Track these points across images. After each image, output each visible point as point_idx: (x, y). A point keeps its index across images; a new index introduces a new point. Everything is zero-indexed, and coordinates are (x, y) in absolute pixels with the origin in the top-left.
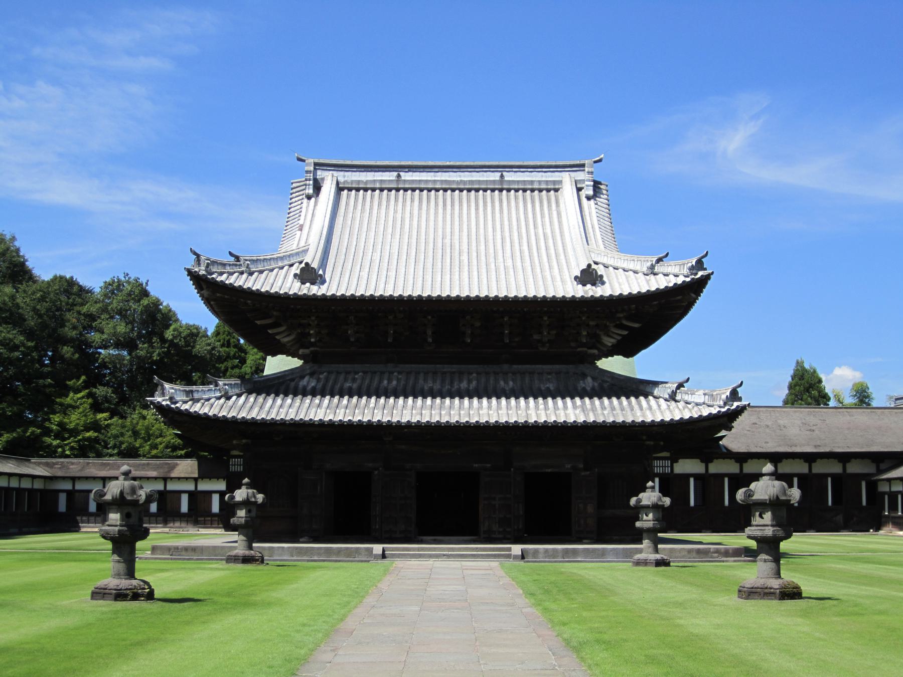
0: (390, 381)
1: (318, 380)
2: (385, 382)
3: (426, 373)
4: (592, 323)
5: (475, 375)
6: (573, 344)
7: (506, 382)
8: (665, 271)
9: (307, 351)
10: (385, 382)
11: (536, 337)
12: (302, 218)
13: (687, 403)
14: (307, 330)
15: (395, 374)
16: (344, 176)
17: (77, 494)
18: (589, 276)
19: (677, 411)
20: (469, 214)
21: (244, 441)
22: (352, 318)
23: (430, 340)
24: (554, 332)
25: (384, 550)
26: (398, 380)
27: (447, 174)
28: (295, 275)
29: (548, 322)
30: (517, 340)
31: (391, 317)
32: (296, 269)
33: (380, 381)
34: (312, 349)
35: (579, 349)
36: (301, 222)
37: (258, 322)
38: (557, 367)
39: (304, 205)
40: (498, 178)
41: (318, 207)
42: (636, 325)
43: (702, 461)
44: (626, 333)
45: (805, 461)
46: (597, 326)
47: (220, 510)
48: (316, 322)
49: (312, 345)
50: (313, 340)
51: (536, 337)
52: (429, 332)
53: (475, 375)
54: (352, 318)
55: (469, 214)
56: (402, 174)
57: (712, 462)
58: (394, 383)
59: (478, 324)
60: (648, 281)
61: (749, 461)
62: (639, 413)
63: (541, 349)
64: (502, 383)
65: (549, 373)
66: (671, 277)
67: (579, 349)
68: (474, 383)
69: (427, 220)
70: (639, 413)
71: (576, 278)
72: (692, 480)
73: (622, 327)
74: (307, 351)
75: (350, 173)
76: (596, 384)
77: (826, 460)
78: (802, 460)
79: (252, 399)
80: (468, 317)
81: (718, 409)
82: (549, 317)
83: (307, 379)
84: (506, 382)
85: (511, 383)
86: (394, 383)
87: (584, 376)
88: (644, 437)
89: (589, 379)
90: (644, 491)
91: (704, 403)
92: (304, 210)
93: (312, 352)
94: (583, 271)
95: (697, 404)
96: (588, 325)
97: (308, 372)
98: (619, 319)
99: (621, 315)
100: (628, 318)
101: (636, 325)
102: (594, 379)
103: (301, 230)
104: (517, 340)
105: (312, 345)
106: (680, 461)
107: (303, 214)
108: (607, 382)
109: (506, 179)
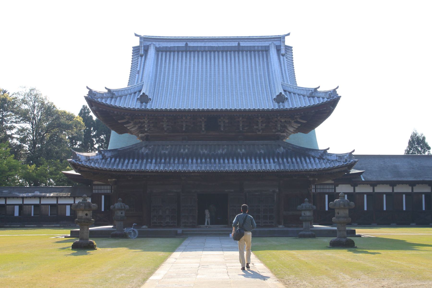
0: (184, 150)
1: (149, 149)
2: (182, 150)
3: (172, 145)
4: (283, 120)
5: (226, 146)
6: (274, 130)
7: (241, 150)
8: (318, 96)
9: (143, 135)
10: (182, 150)
11: (255, 127)
12: (139, 67)
13: (328, 160)
14: (143, 125)
15: (187, 146)
16: (159, 44)
17: (8, 206)
18: (280, 99)
19: (323, 164)
20: (223, 64)
21: (114, 180)
22: (165, 118)
23: (203, 129)
24: (265, 125)
25: (183, 231)
26: (188, 149)
27: (211, 43)
28: (138, 99)
29: (261, 120)
30: (246, 129)
31: (184, 118)
32: (138, 96)
33: (180, 150)
34: (145, 134)
35: (277, 133)
36: (138, 69)
37: (119, 121)
38: (266, 142)
39: (140, 59)
40: (237, 45)
41: (147, 61)
42: (305, 122)
43: (352, 186)
44: (300, 125)
45: (410, 186)
46: (285, 121)
47: (70, 214)
48: (148, 121)
49: (146, 132)
50: (146, 130)
51: (255, 127)
52: (203, 125)
53: (226, 146)
54: (165, 118)
55: (223, 64)
56: (188, 43)
57: (357, 186)
58: (186, 150)
59: (227, 121)
60: (309, 101)
61: (378, 185)
62: (305, 165)
63: (258, 133)
64: (239, 150)
65: (262, 145)
66: (321, 98)
67: (277, 133)
68: (225, 150)
69: (202, 68)
70: (305, 165)
71: (274, 99)
72: (385, 196)
73: (297, 122)
74: (143, 135)
75: (162, 43)
76: (285, 151)
77: (421, 185)
78: (427, 185)
79: (126, 161)
80: (222, 118)
81: (343, 163)
82: (262, 118)
83: (143, 149)
84: (241, 150)
85: (243, 150)
86: (186, 150)
87: (279, 146)
88: (308, 177)
89: (282, 148)
90: (304, 203)
91: (336, 160)
92: (139, 63)
93: (145, 135)
94: (278, 96)
95: (333, 161)
96: (281, 121)
97: (144, 145)
98: (296, 118)
99: (297, 117)
100: (301, 118)
101: (305, 122)
102: (284, 148)
103: (138, 73)
104: (246, 129)
105: (146, 132)
106: (340, 185)
107: (139, 65)
108: (290, 149)
109: (241, 45)
